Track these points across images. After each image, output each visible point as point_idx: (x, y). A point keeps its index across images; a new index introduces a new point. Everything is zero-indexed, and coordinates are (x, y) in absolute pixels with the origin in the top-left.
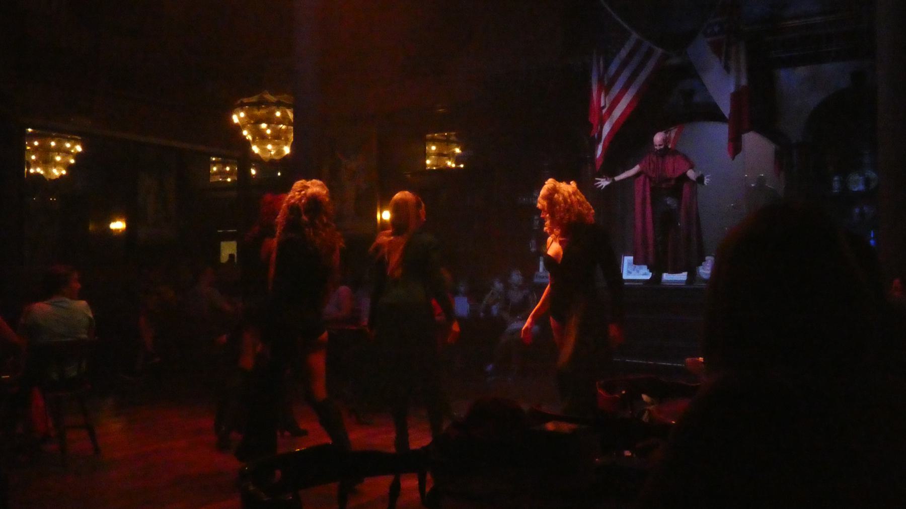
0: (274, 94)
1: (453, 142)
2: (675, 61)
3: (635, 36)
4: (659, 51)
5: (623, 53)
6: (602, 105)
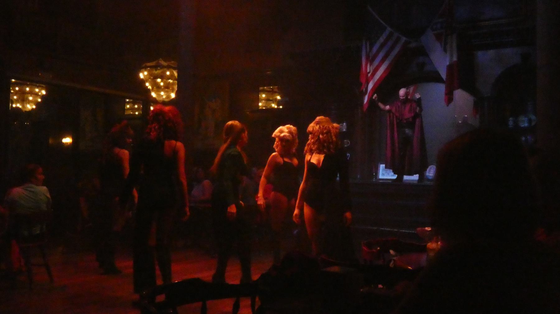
0: (165, 61)
1: (275, 92)
2: (413, 45)
3: (389, 29)
4: (404, 39)
5: (382, 40)
6: (368, 71)
